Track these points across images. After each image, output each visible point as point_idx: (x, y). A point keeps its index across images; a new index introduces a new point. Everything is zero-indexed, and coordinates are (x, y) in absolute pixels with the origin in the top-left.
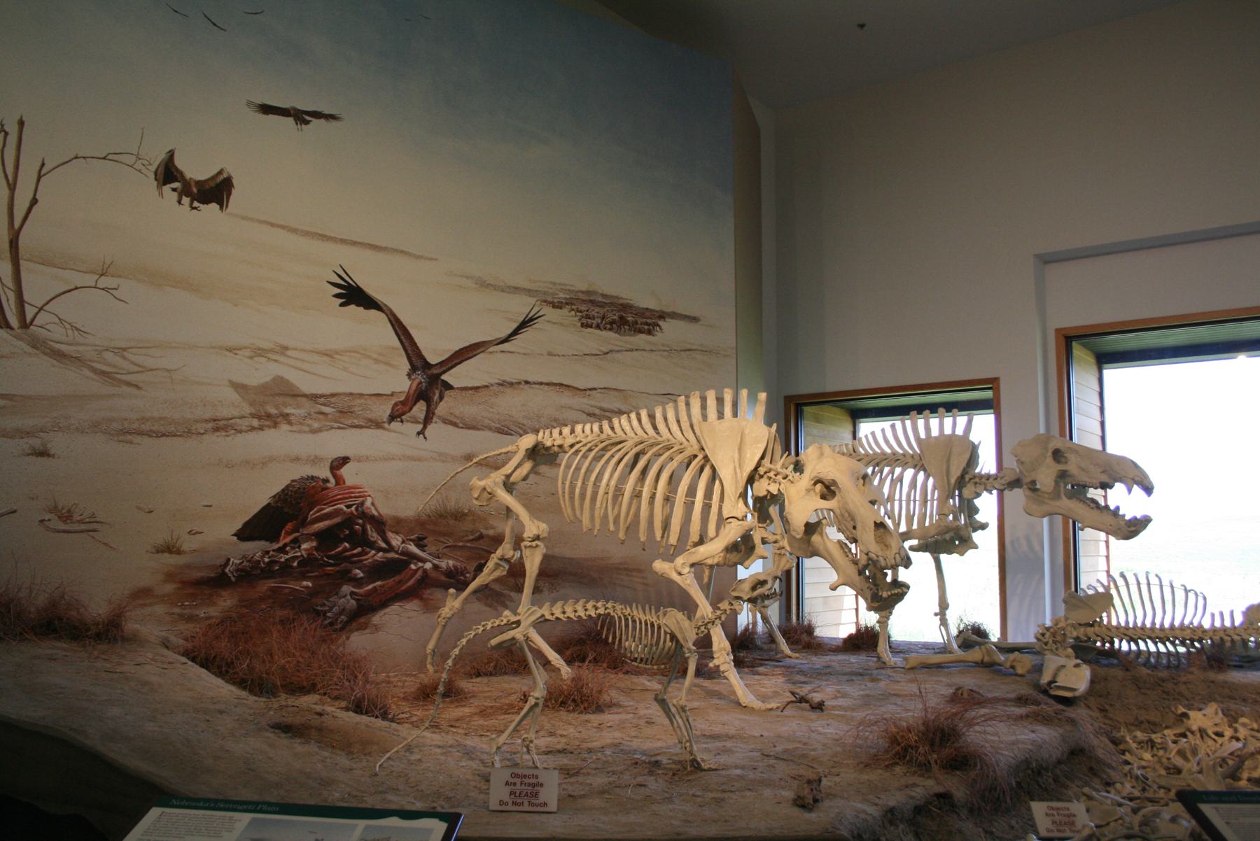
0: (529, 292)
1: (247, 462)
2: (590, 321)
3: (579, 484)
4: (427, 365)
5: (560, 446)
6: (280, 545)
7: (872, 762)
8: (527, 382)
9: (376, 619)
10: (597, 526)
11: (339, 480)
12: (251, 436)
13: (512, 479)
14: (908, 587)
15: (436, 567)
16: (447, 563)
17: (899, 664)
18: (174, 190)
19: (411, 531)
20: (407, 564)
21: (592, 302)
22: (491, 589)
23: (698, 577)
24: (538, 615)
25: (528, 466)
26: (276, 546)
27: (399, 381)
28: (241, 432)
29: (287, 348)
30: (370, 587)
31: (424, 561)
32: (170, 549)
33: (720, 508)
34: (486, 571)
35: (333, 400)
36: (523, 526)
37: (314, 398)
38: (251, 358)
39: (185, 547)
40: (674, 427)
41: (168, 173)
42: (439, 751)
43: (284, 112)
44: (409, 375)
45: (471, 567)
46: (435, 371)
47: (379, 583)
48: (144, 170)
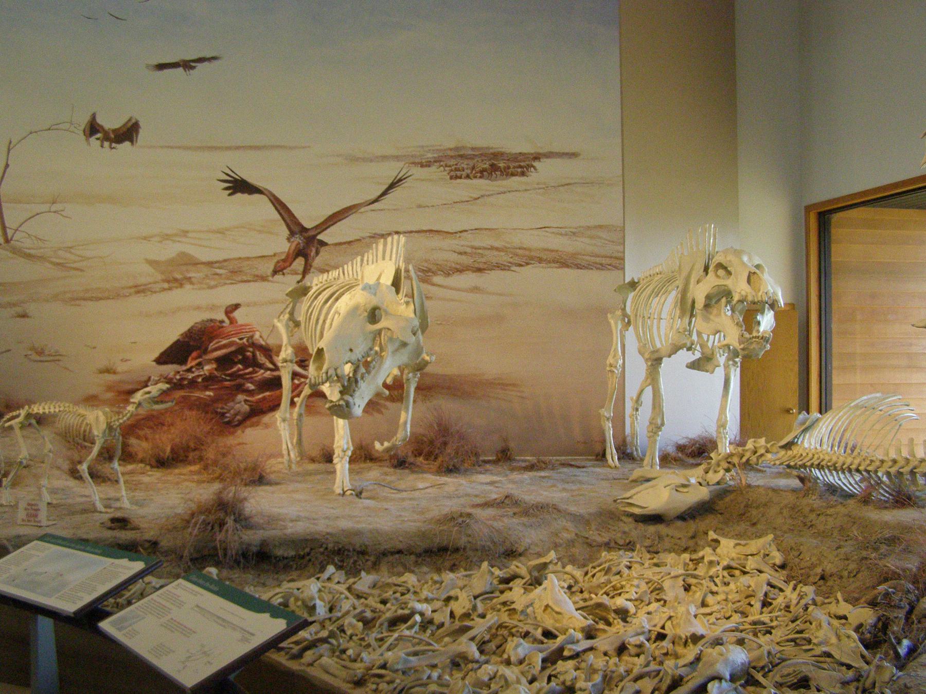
0: (397, 158)
1: (161, 312)
2: (459, 173)
4: (304, 230)
6: (189, 366)
7: (182, 519)
9: (266, 419)
11: (232, 321)
12: (162, 295)
18: (98, 139)
21: (461, 156)
26: (184, 368)
27: (280, 243)
28: (155, 292)
29: (187, 232)
30: (260, 396)
32: (108, 371)
35: (225, 264)
37: (210, 264)
38: (160, 242)
39: (119, 369)
41: (93, 129)
43: (175, 65)
46: (311, 233)
47: (268, 394)
48: (76, 131)
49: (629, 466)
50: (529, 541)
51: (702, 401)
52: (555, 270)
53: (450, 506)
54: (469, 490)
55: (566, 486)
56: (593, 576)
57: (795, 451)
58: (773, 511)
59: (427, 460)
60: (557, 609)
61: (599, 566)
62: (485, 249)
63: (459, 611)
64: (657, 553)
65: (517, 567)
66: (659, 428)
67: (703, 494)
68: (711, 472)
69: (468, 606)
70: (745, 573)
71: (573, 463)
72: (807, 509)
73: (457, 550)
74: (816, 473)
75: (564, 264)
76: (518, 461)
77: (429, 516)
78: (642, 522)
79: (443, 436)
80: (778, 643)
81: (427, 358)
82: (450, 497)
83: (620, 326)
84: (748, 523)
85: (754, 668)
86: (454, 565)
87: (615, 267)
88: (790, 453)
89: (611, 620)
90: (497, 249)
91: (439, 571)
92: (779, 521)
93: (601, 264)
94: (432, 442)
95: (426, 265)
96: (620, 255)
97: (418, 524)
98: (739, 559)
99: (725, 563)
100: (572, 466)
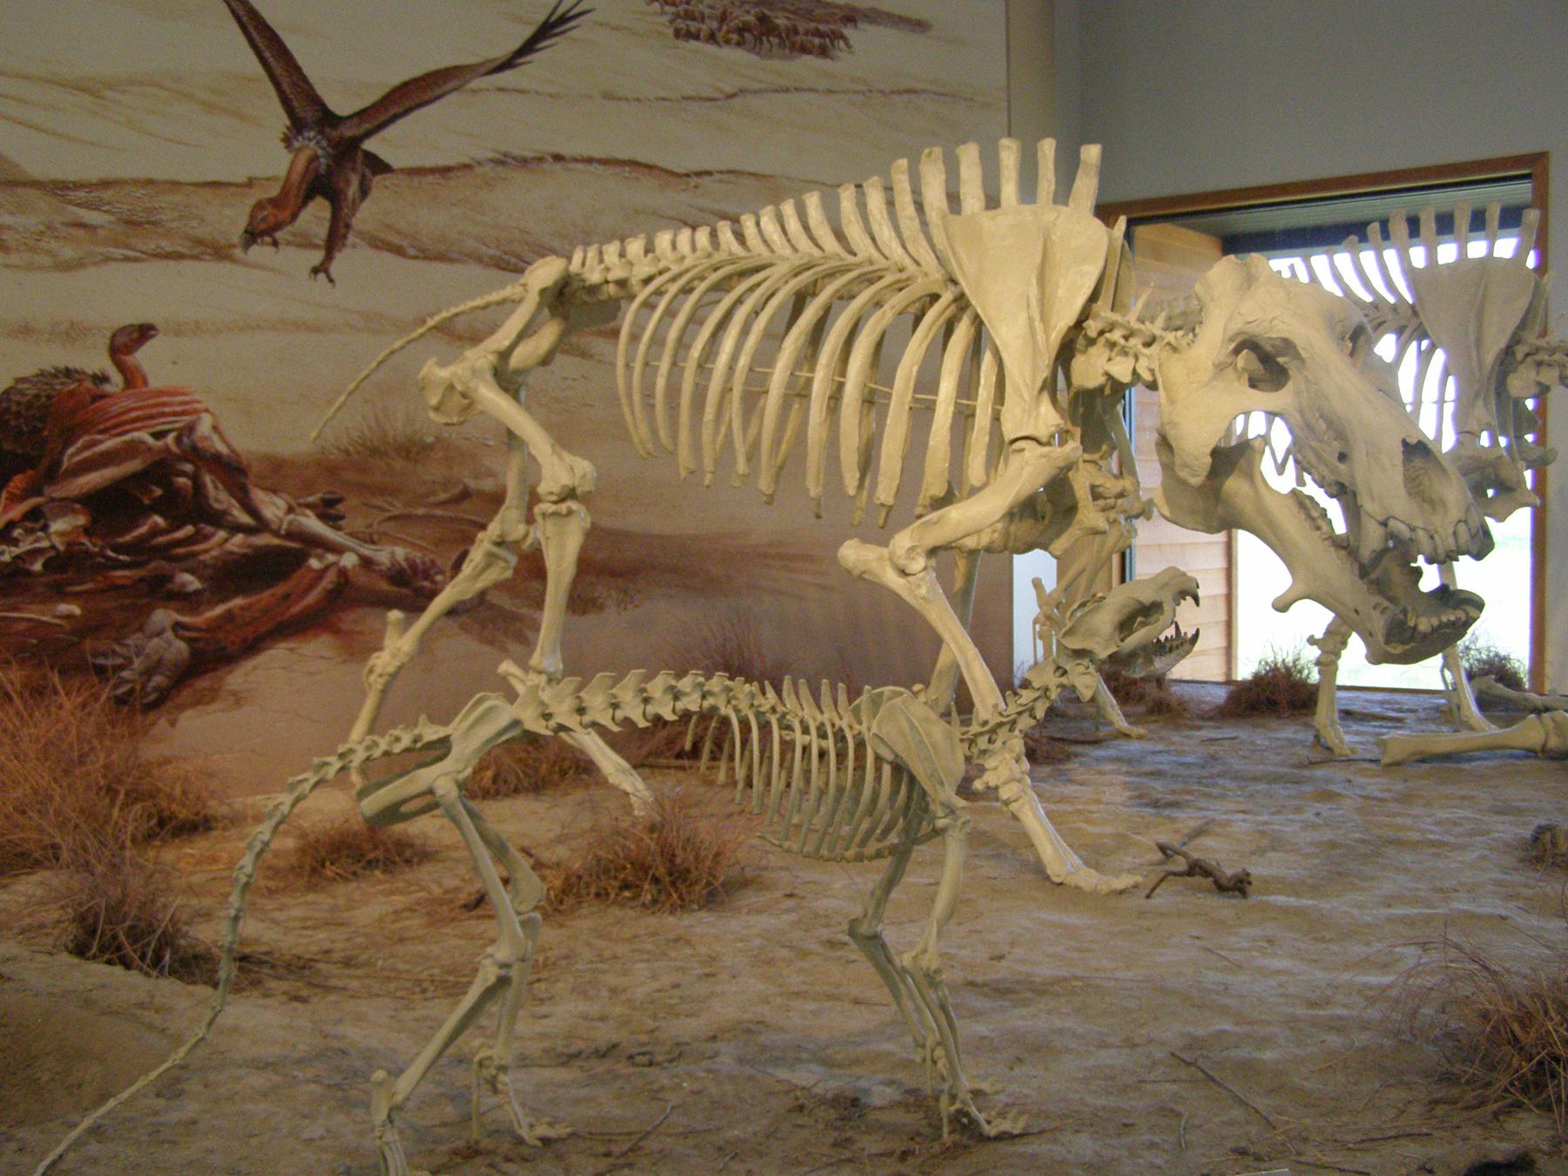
2: (693, 26)
3: (664, 365)
4: (328, 119)
5: (622, 283)
8: (558, 158)
9: (237, 678)
10: (708, 464)
11: (132, 378)
13: (515, 361)
14: (1479, 605)
15: (367, 563)
16: (388, 554)
17: (1361, 752)
19: (308, 487)
20: (299, 559)
22: (492, 606)
23: (944, 577)
24: (502, 721)
25: (548, 334)
27: (266, 153)
30: (219, 610)
31: (338, 550)
33: (996, 419)
34: (467, 569)
35: (107, 195)
36: (538, 467)
37: (59, 189)
40: (885, 233)
42: (257, 1080)
44: (287, 141)
45: (446, 563)
46: (349, 132)
47: (238, 602)
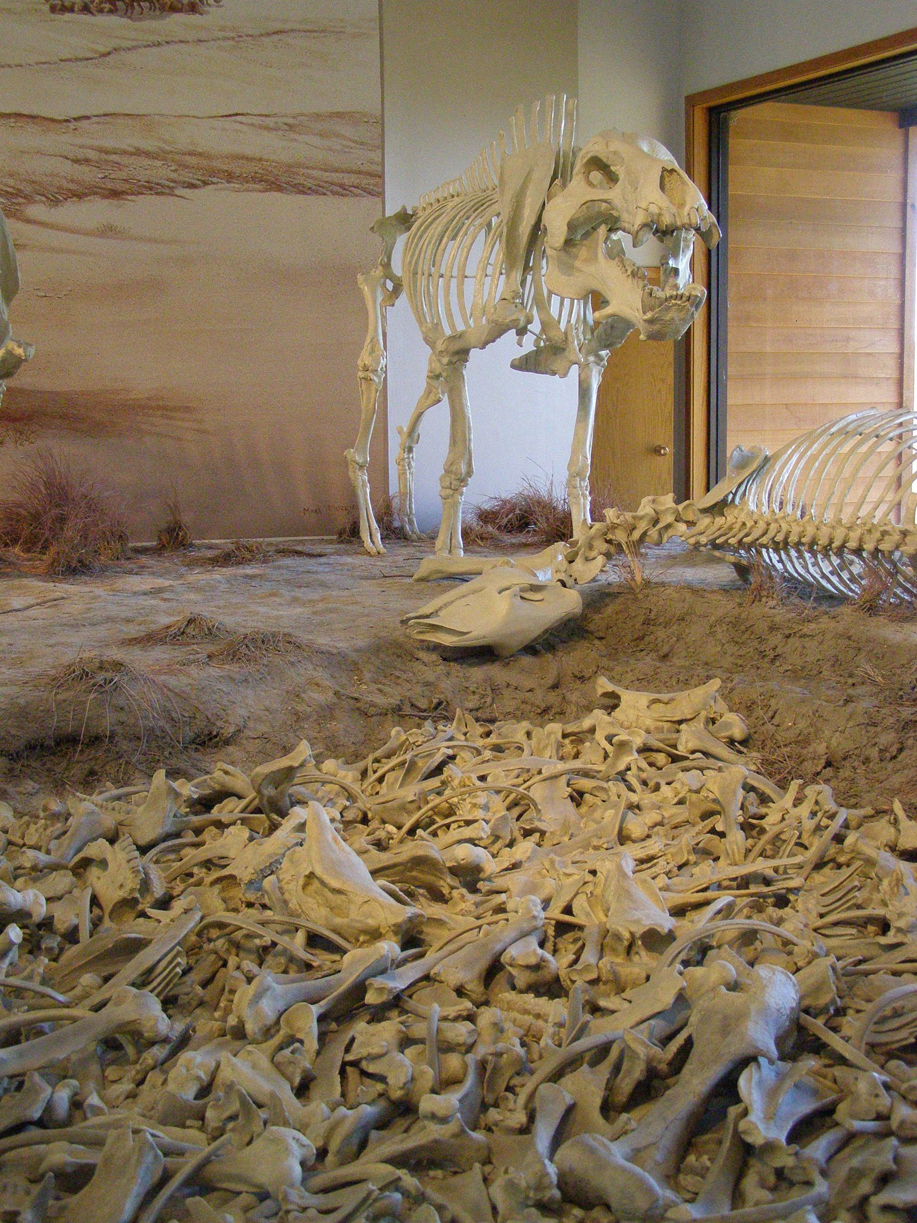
49: (403, 552)
50: (243, 712)
51: (533, 432)
52: (254, 195)
53: (77, 647)
54: (114, 610)
55: (299, 593)
56: (381, 780)
57: (731, 516)
58: (695, 632)
59: (28, 551)
60: (335, 883)
61: (388, 757)
62: (125, 152)
63: (111, 895)
64: (492, 721)
65: (226, 773)
66: (463, 481)
67: (569, 602)
68: (579, 561)
69: (132, 883)
70: (675, 759)
71: (299, 548)
72: (762, 627)
73: (95, 740)
74: (770, 557)
75: (275, 186)
76: (199, 547)
77: (36, 667)
78: (455, 660)
79: (58, 506)
80: (815, 930)
81: (19, 351)
82: (76, 626)
83: (380, 298)
84: (654, 655)
85: (806, 1011)
86: (92, 773)
87: (364, 190)
88: (720, 521)
89: (446, 891)
90: (147, 154)
91: (59, 787)
92: (711, 649)
93: (341, 186)
94: (36, 517)
95: (11, 182)
96: (379, 168)
97: (14, 690)
98: (660, 730)
99: (638, 741)
100: (299, 553)
